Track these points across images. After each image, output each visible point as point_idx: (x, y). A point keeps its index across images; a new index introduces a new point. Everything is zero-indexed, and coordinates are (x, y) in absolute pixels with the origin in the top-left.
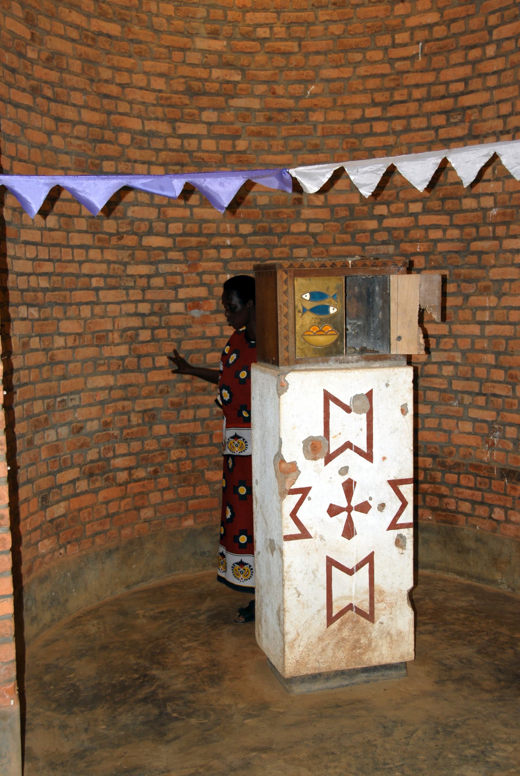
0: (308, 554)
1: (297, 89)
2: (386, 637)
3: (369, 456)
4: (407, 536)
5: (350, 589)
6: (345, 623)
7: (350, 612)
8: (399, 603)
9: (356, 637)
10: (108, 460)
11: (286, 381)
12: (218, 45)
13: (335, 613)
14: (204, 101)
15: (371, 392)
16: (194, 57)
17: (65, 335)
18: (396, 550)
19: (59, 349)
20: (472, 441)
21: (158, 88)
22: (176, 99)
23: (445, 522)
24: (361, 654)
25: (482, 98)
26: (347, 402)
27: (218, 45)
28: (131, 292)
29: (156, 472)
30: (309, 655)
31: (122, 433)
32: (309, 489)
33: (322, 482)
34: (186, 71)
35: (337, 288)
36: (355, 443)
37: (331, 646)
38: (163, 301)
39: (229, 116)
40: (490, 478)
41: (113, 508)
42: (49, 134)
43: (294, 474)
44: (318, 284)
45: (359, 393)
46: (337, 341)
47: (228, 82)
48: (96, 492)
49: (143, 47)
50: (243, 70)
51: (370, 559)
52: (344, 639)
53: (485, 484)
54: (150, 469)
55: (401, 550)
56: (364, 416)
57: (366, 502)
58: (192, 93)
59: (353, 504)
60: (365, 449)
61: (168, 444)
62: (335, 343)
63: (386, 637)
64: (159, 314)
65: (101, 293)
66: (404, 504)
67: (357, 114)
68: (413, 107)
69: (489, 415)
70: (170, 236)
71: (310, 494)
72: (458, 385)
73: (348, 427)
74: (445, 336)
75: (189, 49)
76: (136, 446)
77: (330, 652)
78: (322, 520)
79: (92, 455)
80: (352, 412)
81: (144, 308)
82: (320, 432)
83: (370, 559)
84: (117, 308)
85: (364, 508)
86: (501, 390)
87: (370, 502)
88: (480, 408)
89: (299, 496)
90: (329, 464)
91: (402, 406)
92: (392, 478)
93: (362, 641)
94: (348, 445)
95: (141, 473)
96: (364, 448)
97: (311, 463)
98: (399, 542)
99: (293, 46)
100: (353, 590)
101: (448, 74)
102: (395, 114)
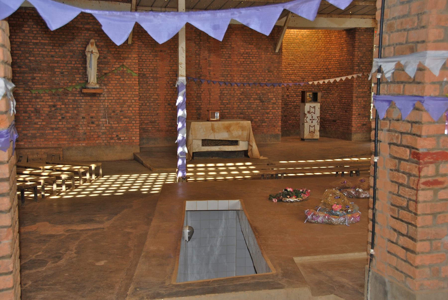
1: (304, 63)
5: (312, 129)
12: (293, 57)
14: (290, 65)
16: (289, 59)
20: (329, 116)
25: (331, 67)
27: (293, 57)
33: (309, 116)
39: (294, 67)
44: (309, 93)
50: (296, 61)
58: (289, 64)
69: (331, 112)
72: (327, 108)
73: (312, 110)
86: (333, 109)
99: (303, 57)
101: (326, 63)
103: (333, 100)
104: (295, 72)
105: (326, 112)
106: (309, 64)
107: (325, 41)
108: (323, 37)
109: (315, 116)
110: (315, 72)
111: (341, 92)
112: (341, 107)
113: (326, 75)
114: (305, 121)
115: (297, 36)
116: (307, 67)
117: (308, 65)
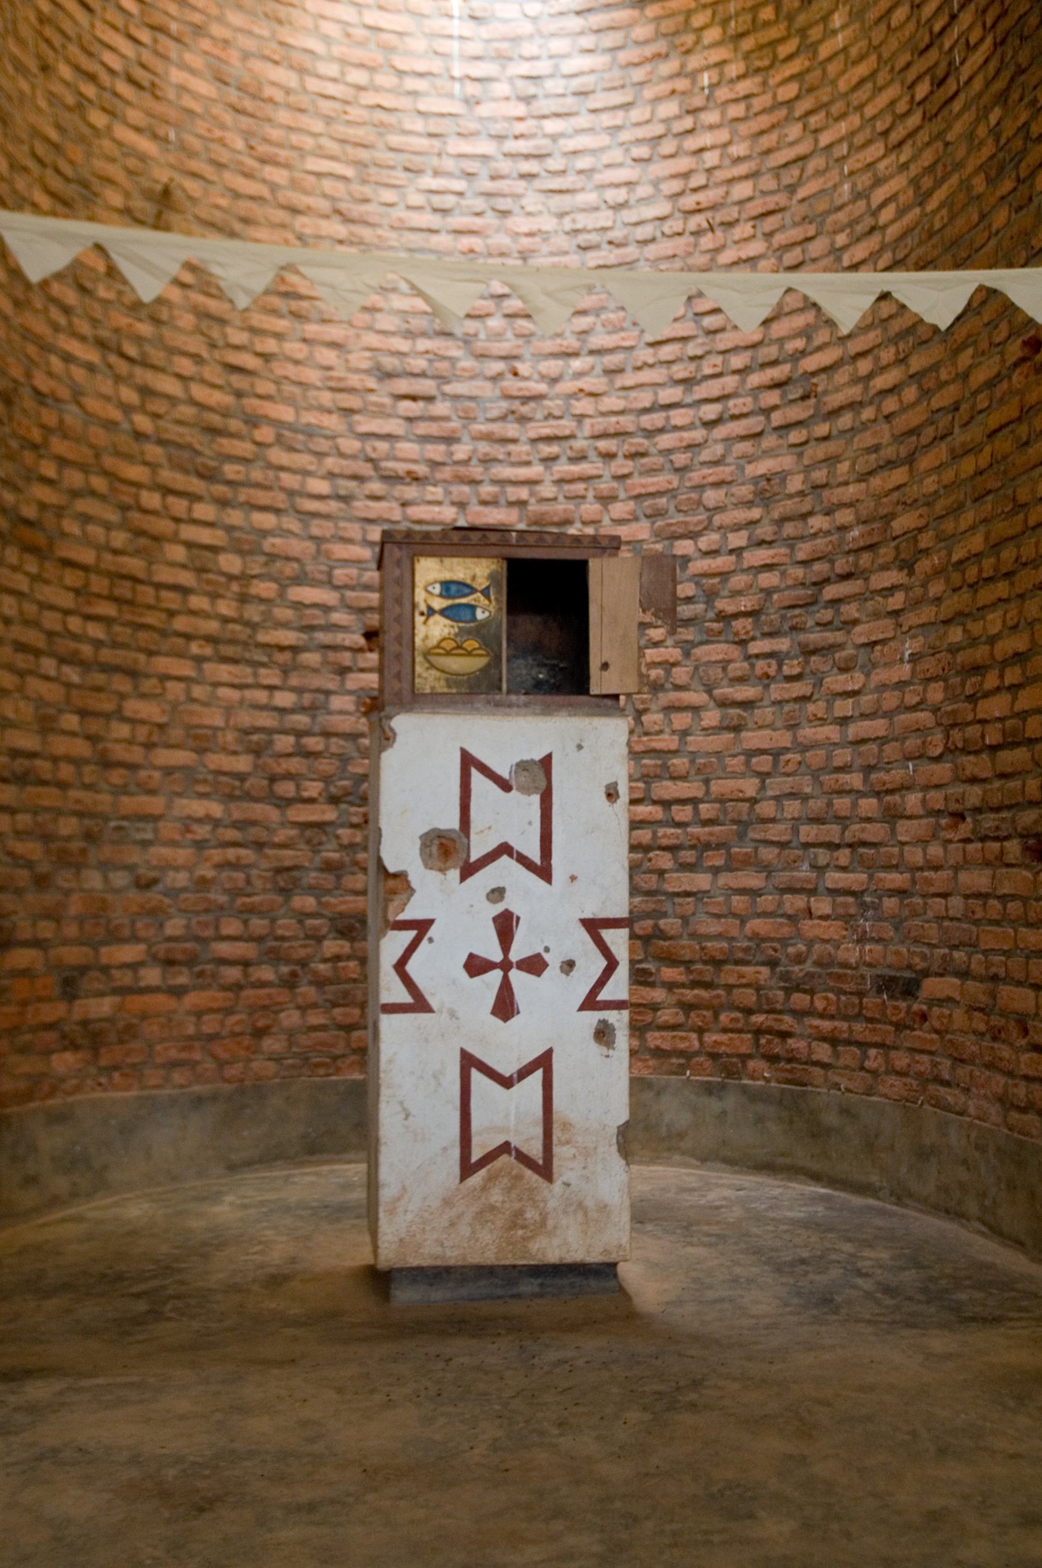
0: (426, 1040)
1: (552, 367)
2: (575, 1212)
3: (544, 872)
4: (616, 1025)
5: (507, 1114)
6: (496, 1177)
7: (504, 1159)
8: (600, 1150)
9: (517, 1206)
10: (204, 941)
11: (392, 730)
13: (476, 1156)
15: (549, 757)
16: (385, 322)
17: (132, 721)
18: (595, 1049)
19: (117, 741)
20: (833, 930)
21: (326, 363)
22: (354, 380)
23: (788, 1082)
24: (525, 1239)
26: (504, 772)
28: (263, 671)
29: (294, 974)
30: (424, 1230)
31: (232, 901)
32: (430, 922)
33: (454, 912)
34: (372, 339)
35: (492, 577)
36: (518, 846)
37: (467, 1218)
38: (318, 691)
39: (441, 408)
40: (861, 994)
41: (210, 1024)
42: (127, 409)
43: (404, 896)
44: (459, 569)
45: (527, 757)
46: (488, 665)
47: (444, 358)
48: (178, 992)
49: (305, 304)
50: (468, 340)
51: (544, 1062)
52: (492, 1208)
53: (853, 1006)
54: (285, 969)
55: (604, 1050)
56: (536, 799)
57: (538, 956)
59: (514, 956)
60: (536, 857)
61: (317, 929)
62: (485, 670)
63: (575, 1212)
64: (311, 710)
65: (208, 667)
66: (612, 965)
67: (645, 399)
68: (730, 382)
69: (856, 879)
70: (336, 588)
71: (432, 932)
73: (504, 818)
74: (787, 750)
75: (379, 310)
76: (258, 925)
77: (464, 1230)
78: (454, 983)
79: (175, 926)
80: (514, 792)
81: (284, 699)
82: (451, 822)
83: (544, 1062)
84: (234, 695)
85: (535, 965)
86: (875, 832)
87: (547, 957)
88: (844, 869)
89: (411, 934)
90: (470, 881)
91: (608, 787)
92: (588, 915)
93: (528, 1215)
94: (505, 849)
95: (266, 973)
96: (535, 855)
97: (434, 875)
98: (603, 1034)
100: (512, 1118)
102: (704, 395)
103: (878, 727)
104: (461, 451)
105: (804, 873)
106: (611, 372)
107: (765, 100)
108: (734, 70)
109: (550, 918)
110: (666, 441)
111: (960, 601)
112: (974, 794)
113: (787, 461)
114: (392, 991)
115: (473, 102)
116: (583, 406)
117: (595, 382)
